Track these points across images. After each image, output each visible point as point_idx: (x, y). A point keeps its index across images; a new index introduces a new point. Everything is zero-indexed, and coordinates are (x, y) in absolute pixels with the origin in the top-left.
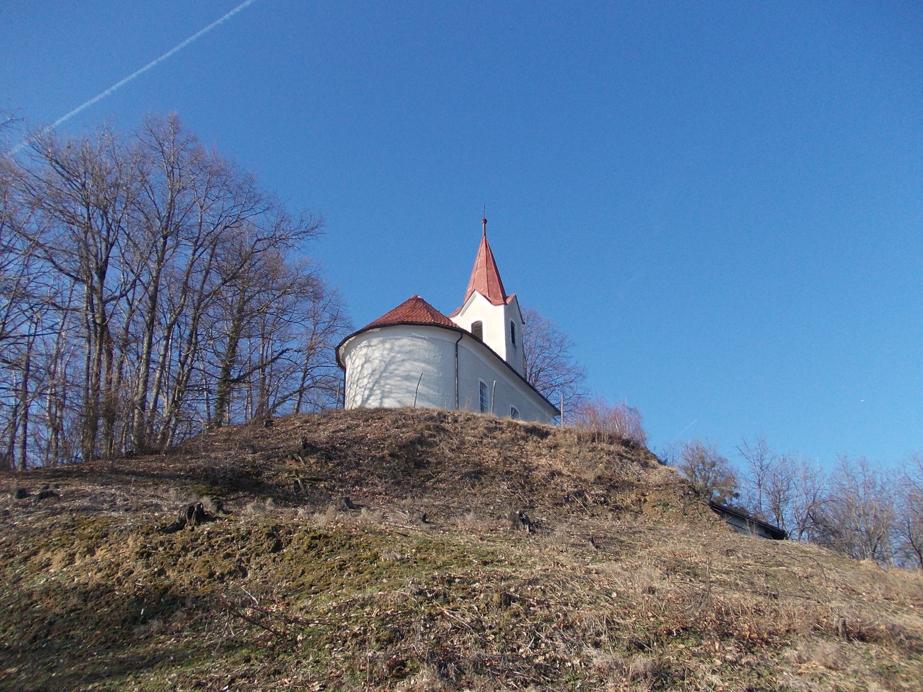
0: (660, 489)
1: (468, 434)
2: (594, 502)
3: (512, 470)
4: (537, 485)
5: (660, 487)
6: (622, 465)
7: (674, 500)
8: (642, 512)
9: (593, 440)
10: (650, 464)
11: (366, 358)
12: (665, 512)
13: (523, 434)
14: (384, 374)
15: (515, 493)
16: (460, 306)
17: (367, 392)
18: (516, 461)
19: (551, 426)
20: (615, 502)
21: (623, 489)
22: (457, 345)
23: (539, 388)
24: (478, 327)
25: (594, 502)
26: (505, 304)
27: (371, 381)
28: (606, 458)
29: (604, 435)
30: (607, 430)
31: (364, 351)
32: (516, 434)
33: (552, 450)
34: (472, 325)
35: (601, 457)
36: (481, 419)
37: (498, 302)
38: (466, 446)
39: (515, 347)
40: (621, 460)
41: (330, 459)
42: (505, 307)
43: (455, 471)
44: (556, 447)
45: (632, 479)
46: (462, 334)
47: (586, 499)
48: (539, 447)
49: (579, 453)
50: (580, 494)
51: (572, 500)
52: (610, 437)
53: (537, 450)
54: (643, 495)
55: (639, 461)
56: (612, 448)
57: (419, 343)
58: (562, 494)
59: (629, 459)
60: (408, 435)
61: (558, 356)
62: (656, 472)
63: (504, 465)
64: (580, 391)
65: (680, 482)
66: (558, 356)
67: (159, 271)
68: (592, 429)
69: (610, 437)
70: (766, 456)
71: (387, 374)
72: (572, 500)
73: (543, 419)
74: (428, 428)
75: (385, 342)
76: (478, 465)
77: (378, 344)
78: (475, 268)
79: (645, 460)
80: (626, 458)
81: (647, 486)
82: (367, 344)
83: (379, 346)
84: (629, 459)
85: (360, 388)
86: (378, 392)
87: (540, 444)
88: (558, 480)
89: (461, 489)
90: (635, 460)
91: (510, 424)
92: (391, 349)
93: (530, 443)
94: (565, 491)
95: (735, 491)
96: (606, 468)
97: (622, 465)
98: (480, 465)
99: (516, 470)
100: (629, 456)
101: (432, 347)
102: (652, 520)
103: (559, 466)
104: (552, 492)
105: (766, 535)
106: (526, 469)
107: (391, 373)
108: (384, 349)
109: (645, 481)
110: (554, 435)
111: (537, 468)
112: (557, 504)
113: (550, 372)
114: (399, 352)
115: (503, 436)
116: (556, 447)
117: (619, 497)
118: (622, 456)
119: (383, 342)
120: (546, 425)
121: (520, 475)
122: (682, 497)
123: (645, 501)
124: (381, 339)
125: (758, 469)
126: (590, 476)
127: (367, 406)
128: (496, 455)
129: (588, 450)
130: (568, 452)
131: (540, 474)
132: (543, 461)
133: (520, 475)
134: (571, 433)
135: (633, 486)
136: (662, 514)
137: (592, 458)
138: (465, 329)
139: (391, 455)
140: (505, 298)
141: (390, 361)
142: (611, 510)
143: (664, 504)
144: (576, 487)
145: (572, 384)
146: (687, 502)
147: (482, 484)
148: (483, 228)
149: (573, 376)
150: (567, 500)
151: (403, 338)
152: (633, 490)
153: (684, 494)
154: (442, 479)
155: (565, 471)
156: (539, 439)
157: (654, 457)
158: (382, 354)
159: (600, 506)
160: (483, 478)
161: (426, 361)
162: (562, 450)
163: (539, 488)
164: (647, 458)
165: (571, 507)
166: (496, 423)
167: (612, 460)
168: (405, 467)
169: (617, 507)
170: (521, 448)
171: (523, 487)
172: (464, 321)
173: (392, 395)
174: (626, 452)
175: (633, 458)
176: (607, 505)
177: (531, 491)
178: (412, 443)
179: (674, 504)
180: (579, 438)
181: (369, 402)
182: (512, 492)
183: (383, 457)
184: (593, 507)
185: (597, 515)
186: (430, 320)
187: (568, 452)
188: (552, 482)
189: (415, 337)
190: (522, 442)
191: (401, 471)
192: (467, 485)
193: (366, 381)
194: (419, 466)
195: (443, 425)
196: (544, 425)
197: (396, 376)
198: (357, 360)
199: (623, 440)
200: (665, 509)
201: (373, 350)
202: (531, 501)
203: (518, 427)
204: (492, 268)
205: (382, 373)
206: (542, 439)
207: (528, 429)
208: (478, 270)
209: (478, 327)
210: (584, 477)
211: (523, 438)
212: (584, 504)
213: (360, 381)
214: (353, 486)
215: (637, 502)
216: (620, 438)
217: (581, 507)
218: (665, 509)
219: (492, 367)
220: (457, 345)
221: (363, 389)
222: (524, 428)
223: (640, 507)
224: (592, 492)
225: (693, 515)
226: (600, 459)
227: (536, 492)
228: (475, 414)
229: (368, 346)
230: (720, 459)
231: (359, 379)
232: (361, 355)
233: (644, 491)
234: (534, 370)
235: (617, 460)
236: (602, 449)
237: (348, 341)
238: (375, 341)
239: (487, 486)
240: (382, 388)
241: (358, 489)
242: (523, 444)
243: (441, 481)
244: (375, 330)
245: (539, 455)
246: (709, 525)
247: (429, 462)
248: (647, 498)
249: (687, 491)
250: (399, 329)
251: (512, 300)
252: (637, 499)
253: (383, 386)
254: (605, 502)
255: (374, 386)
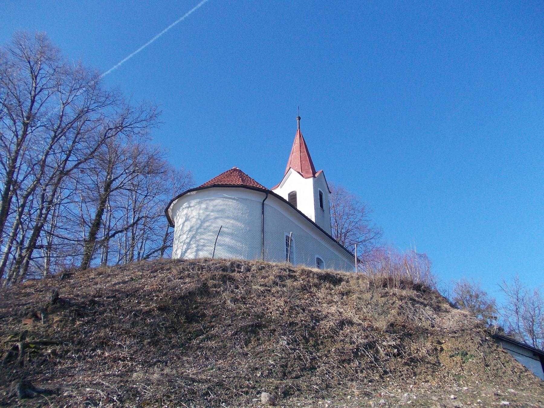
0: (456, 335)
1: (256, 283)
2: (387, 355)
3: (297, 320)
4: (324, 337)
5: (455, 333)
6: (415, 310)
7: (472, 348)
8: (440, 363)
9: (385, 286)
10: (443, 308)
11: (186, 218)
12: (464, 362)
13: (316, 281)
14: (199, 231)
15: (295, 350)
16: (280, 179)
17: (185, 246)
18: (304, 310)
19: (345, 273)
20: (410, 354)
21: (418, 337)
22: (263, 204)
23: (346, 245)
24: (293, 196)
25: (387, 355)
26: (314, 176)
27: (188, 236)
28: (399, 303)
29: (396, 280)
30: (397, 276)
31: (185, 211)
32: (309, 282)
33: (344, 297)
34: (289, 194)
35: (394, 303)
36: (275, 268)
37: (308, 176)
38: (252, 296)
39: (323, 211)
40: (413, 305)
41: (80, 315)
42: (313, 179)
43: (230, 325)
44: (348, 293)
45: (426, 324)
46: (267, 195)
47: (377, 351)
48: (331, 294)
49: (371, 298)
50: (370, 346)
51: (362, 355)
52: (402, 282)
53: (329, 297)
54: (439, 343)
55: (431, 305)
56: (404, 293)
57: (232, 203)
58: (351, 347)
59: (422, 303)
60: (190, 285)
61: (360, 220)
62: (449, 316)
63: (290, 316)
64: (378, 245)
65: (475, 327)
66: (360, 220)
67: (17, 152)
68: (384, 274)
69: (402, 282)
70: (520, 291)
71: (202, 230)
72: (362, 355)
73: (337, 267)
74: (213, 278)
75: (202, 203)
76: (258, 317)
77: (196, 205)
78: (291, 152)
79: (437, 304)
80: (418, 302)
81: (443, 333)
82: (188, 206)
83: (196, 206)
84: (422, 303)
85: (180, 243)
86: (194, 245)
87: (333, 291)
88: (347, 330)
89: (231, 348)
90: (427, 304)
91: (303, 272)
92: (206, 209)
93: (323, 290)
94: (354, 343)
95: (493, 315)
96: (399, 314)
97: (415, 310)
98: (261, 316)
99: (302, 321)
100: (422, 300)
101: (240, 206)
102: (452, 374)
103: (349, 313)
104: (339, 346)
105: (534, 357)
106: (312, 317)
107: (205, 229)
108: (200, 209)
109: (439, 327)
110: (347, 282)
111: (326, 317)
112: (344, 361)
113: (355, 232)
114: (213, 211)
115: (295, 283)
116: (348, 293)
117: (414, 346)
118: (414, 300)
119: (200, 203)
120: (340, 272)
121: (306, 327)
122: (481, 344)
123: (442, 349)
124: (198, 200)
125: (515, 300)
126: (382, 324)
127: (185, 258)
128: (282, 304)
129: (380, 295)
130: (360, 298)
131: (327, 324)
132: (333, 309)
133: (306, 327)
134: (363, 279)
135: (427, 333)
136: (461, 366)
137: (385, 304)
138: (282, 196)
139: (160, 309)
140: (314, 173)
141: (204, 219)
142: (406, 364)
143: (462, 354)
144: (367, 337)
145: (372, 241)
146: (487, 350)
147: (258, 340)
148: (298, 123)
149: (372, 235)
150: (356, 354)
151: (216, 199)
152: (428, 337)
153: (482, 341)
154: (212, 335)
155: (355, 320)
156: (332, 286)
157: (446, 300)
158: (199, 214)
159: (393, 358)
160: (261, 332)
161: (236, 218)
162: (355, 296)
163: (325, 340)
164: (439, 302)
165: (360, 363)
166: (290, 270)
167: (405, 306)
168: (172, 322)
169: (412, 360)
170: (312, 295)
171: (307, 341)
172: (283, 192)
173: (205, 248)
174: (418, 296)
175: (426, 302)
176: (401, 357)
177: (316, 345)
178: (191, 294)
179: (472, 353)
180: (371, 283)
181: (186, 255)
182: (291, 349)
183: (150, 311)
184: (386, 360)
185: (391, 371)
186: (240, 183)
187: (360, 298)
188: (341, 333)
189: (226, 198)
190: (314, 289)
191: (166, 328)
192: (239, 342)
193: (185, 236)
194: (191, 320)
195: (233, 274)
196: (338, 272)
197: (209, 231)
198: (180, 219)
199: (415, 285)
200: (464, 359)
201: (192, 210)
202: (314, 359)
203: (311, 275)
204: (304, 152)
205: (198, 229)
206: (335, 286)
207: (322, 276)
208: (294, 154)
209: (293, 196)
210: (376, 325)
211: (315, 285)
212: (375, 358)
213: (181, 237)
214: (94, 350)
215: (433, 351)
216: (412, 283)
217: (371, 362)
218: (464, 359)
219: (303, 227)
220: (263, 204)
221: (182, 244)
222: (317, 275)
223: (437, 357)
224: (384, 343)
225: (495, 366)
226: (392, 304)
227: (321, 347)
228: (270, 263)
229: (188, 207)
230: (482, 292)
231: (180, 235)
232: (183, 215)
233: (440, 338)
234: (343, 231)
235: (410, 305)
236: (394, 294)
237: (172, 205)
238: (193, 203)
239: (263, 343)
240: (197, 243)
241: (100, 353)
242: (314, 291)
243: (209, 338)
244: (192, 193)
245: (330, 302)
246: (516, 378)
247: (204, 315)
248: (444, 346)
249: (484, 336)
250: (213, 191)
251: (320, 174)
252: (433, 348)
253: (198, 241)
254: (399, 354)
255: (191, 241)
